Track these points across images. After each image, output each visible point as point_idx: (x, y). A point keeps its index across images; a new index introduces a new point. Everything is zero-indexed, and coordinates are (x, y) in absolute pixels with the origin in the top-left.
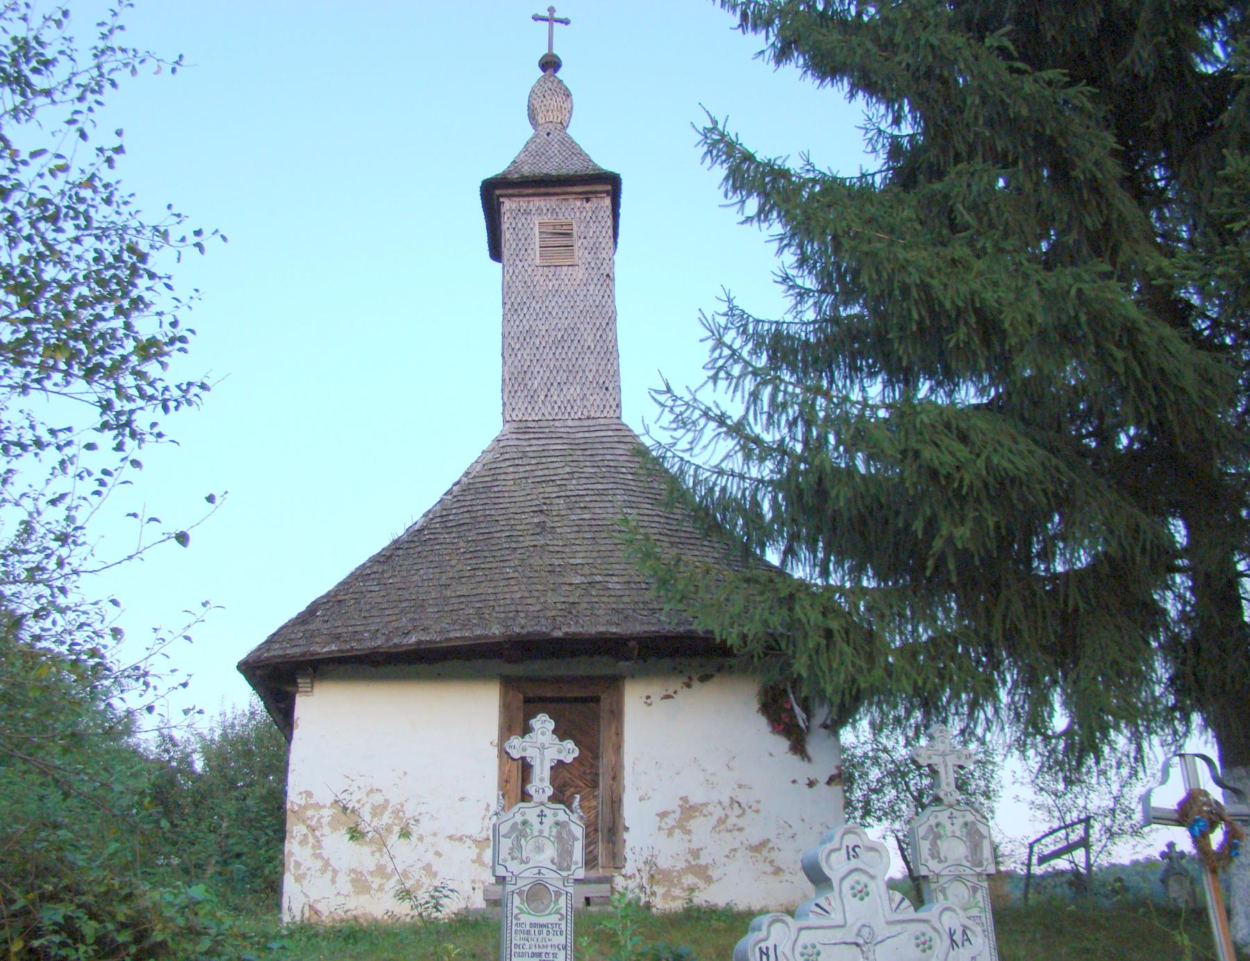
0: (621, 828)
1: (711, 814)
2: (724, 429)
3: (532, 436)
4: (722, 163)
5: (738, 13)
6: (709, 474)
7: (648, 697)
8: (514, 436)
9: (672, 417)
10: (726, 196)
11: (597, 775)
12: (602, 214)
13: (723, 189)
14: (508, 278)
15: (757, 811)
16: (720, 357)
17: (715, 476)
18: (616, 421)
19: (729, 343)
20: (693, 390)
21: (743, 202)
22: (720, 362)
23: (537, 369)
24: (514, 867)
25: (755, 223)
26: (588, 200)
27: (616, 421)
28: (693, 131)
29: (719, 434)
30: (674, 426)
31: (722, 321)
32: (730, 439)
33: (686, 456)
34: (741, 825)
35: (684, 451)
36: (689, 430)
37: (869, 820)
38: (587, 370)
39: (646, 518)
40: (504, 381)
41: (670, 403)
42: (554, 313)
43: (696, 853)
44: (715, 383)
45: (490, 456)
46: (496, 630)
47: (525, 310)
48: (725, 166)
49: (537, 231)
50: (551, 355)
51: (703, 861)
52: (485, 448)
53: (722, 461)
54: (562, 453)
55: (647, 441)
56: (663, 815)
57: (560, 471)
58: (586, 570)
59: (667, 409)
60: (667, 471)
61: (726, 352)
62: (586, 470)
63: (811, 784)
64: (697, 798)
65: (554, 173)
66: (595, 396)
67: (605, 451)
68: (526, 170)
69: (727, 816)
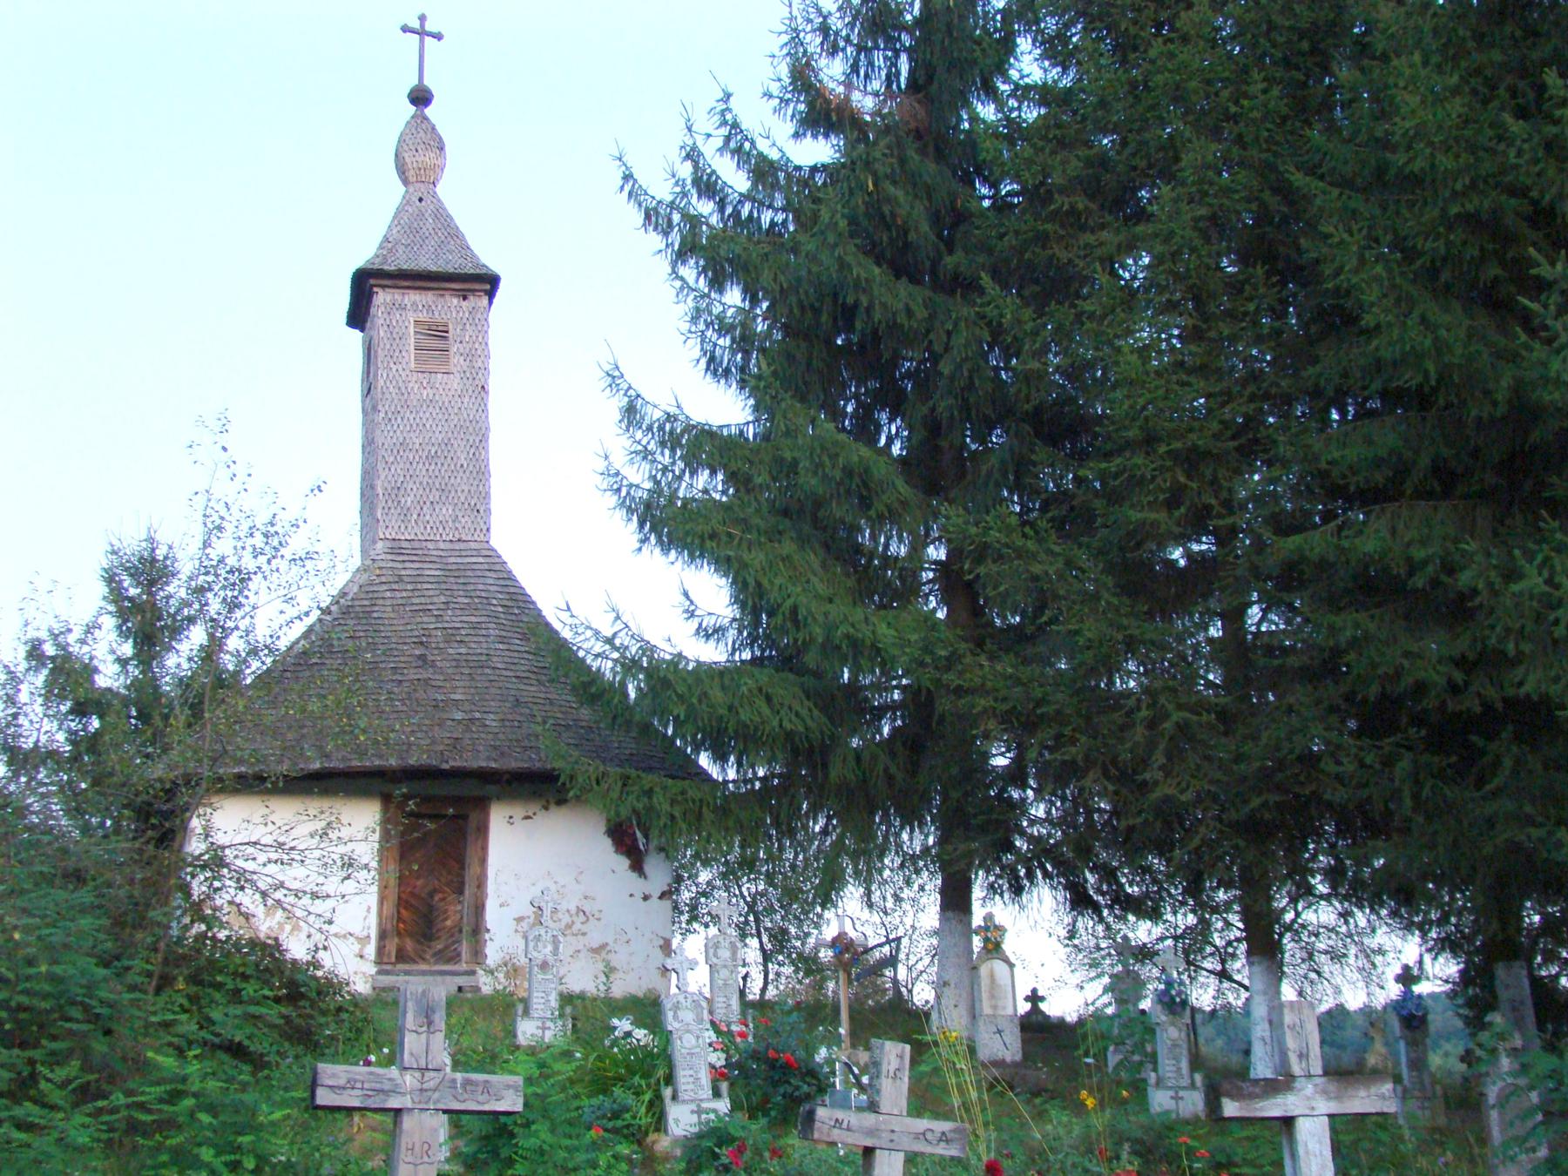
24: (535, 954)
26: (465, 298)
37: (696, 925)
46: (393, 762)
49: (412, 330)
56: (519, 920)
57: (435, 600)
58: (467, 707)
63: (646, 898)
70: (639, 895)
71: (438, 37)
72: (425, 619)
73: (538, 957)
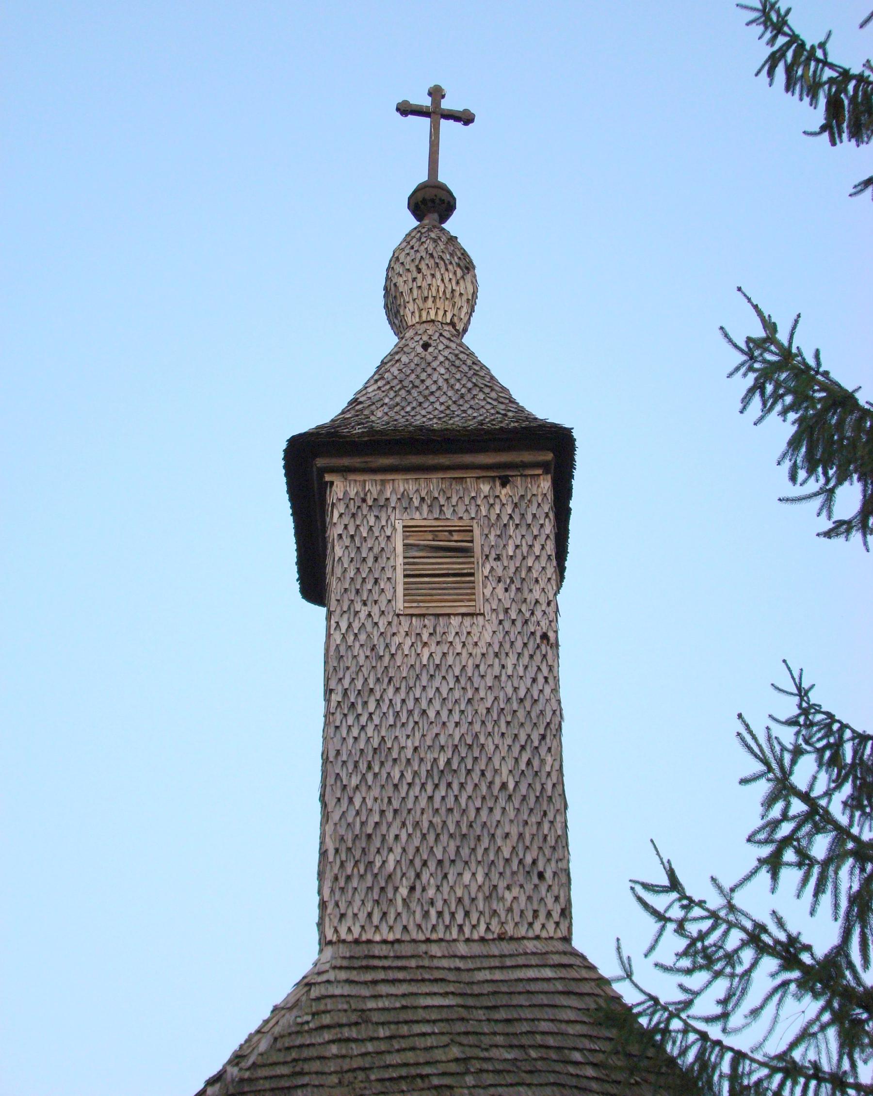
2: (796, 974)
3: (381, 975)
4: (784, 413)
5: (822, 101)
6: (765, 1071)
8: (343, 975)
9: (682, 944)
10: (793, 478)
12: (533, 509)
13: (787, 464)
14: (337, 638)
16: (785, 817)
17: (778, 1077)
18: (561, 946)
19: (803, 787)
20: (727, 885)
21: (829, 494)
22: (786, 829)
23: (394, 831)
25: (856, 536)
27: (561, 946)
28: (724, 342)
29: (785, 984)
30: (686, 963)
31: (787, 736)
32: (808, 998)
33: (714, 1032)
35: (708, 1020)
36: (718, 974)
38: (499, 833)
40: (323, 854)
41: (676, 913)
42: (432, 714)
44: (775, 876)
45: (289, 1018)
47: (372, 706)
48: (792, 416)
49: (399, 542)
50: (423, 802)
52: (278, 998)
53: (793, 1045)
54: (444, 1014)
55: (629, 995)
57: (439, 1055)
59: (671, 927)
60: (671, 1061)
61: (798, 807)
62: (494, 1053)
65: (436, 424)
66: (516, 891)
67: (537, 1013)
68: (379, 417)
71: (466, 118)
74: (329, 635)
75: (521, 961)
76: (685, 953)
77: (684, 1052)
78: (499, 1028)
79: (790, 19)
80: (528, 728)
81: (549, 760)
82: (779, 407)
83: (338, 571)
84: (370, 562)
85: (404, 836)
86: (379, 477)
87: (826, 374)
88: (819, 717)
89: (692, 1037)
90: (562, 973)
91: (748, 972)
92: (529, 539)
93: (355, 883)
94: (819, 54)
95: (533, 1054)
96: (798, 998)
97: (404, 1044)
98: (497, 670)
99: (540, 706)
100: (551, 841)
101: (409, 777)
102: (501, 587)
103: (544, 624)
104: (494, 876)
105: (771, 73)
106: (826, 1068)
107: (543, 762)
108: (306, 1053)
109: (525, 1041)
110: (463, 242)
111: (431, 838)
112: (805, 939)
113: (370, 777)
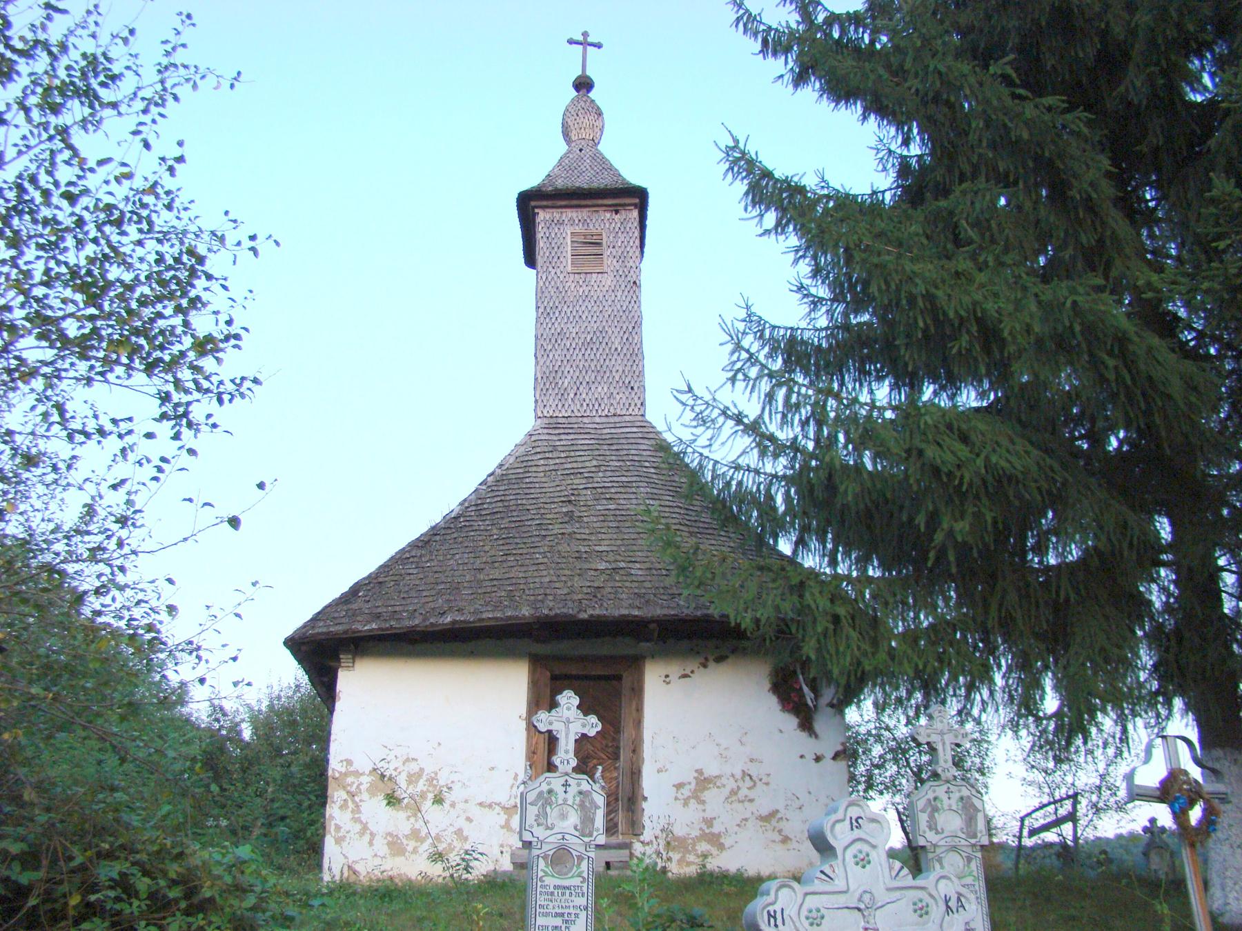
0: (640, 798)
1: (724, 786)
2: (741, 427)
3: (562, 431)
4: (743, 179)
5: (760, 40)
7: (667, 676)
8: (546, 431)
10: (746, 210)
11: (618, 748)
12: (630, 225)
13: (743, 204)
14: (541, 283)
15: (767, 784)
16: (738, 360)
17: (732, 470)
18: (641, 418)
21: (761, 216)
22: (739, 365)
23: (567, 369)
24: (540, 832)
25: (773, 236)
26: (617, 212)
27: (641, 418)
29: (736, 431)
30: (694, 423)
33: (706, 452)
34: (751, 797)
35: (703, 447)
36: (708, 428)
37: (871, 793)
38: (614, 370)
39: (667, 509)
40: (536, 379)
42: (584, 317)
43: (709, 822)
44: (733, 384)
45: (522, 449)
46: (526, 612)
48: (746, 182)
51: (715, 830)
53: (738, 457)
54: (590, 447)
55: (669, 438)
56: (679, 786)
57: (587, 464)
58: (611, 557)
60: (687, 465)
62: (611, 463)
63: (818, 759)
64: (711, 770)
65: (586, 186)
66: (621, 395)
67: (630, 447)
68: (560, 183)
69: (739, 788)
70: (810, 757)
71: (599, 46)
72: (576, 481)
73: (548, 840)
74: (537, 282)
75: (624, 425)
76: (694, 419)
77: (692, 461)
78: (614, 453)
79: (369, 825)
80: (627, 324)
81: (636, 337)
82: (740, 177)
83: (541, 253)
84: (556, 249)
85: (572, 371)
86: (560, 210)
87: (760, 162)
88: (755, 318)
89: (696, 455)
90: (641, 430)
91: (720, 427)
92: (628, 239)
93: (550, 391)
94: (758, 18)
95: (628, 463)
96: (742, 437)
97: (572, 460)
98: (613, 297)
99: (632, 314)
100: (637, 373)
101: (574, 346)
102: (615, 260)
103: (634, 276)
104: (612, 388)
105: (737, 26)
106: (752, 466)
107: (633, 338)
108: (530, 463)
109: (625, 458)
110: (598, 102)
111: (584, 372)
112: (745, 413)
113: (556, 345)
